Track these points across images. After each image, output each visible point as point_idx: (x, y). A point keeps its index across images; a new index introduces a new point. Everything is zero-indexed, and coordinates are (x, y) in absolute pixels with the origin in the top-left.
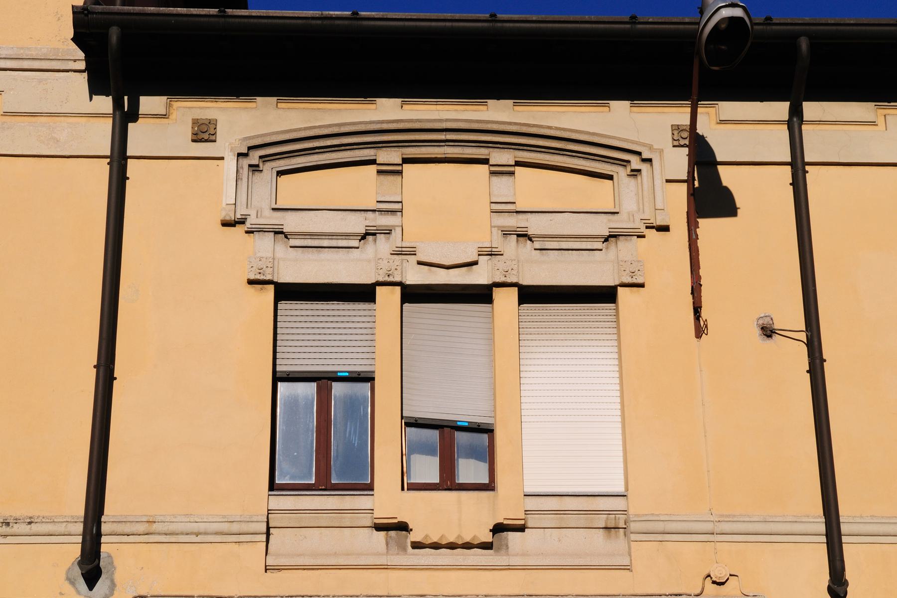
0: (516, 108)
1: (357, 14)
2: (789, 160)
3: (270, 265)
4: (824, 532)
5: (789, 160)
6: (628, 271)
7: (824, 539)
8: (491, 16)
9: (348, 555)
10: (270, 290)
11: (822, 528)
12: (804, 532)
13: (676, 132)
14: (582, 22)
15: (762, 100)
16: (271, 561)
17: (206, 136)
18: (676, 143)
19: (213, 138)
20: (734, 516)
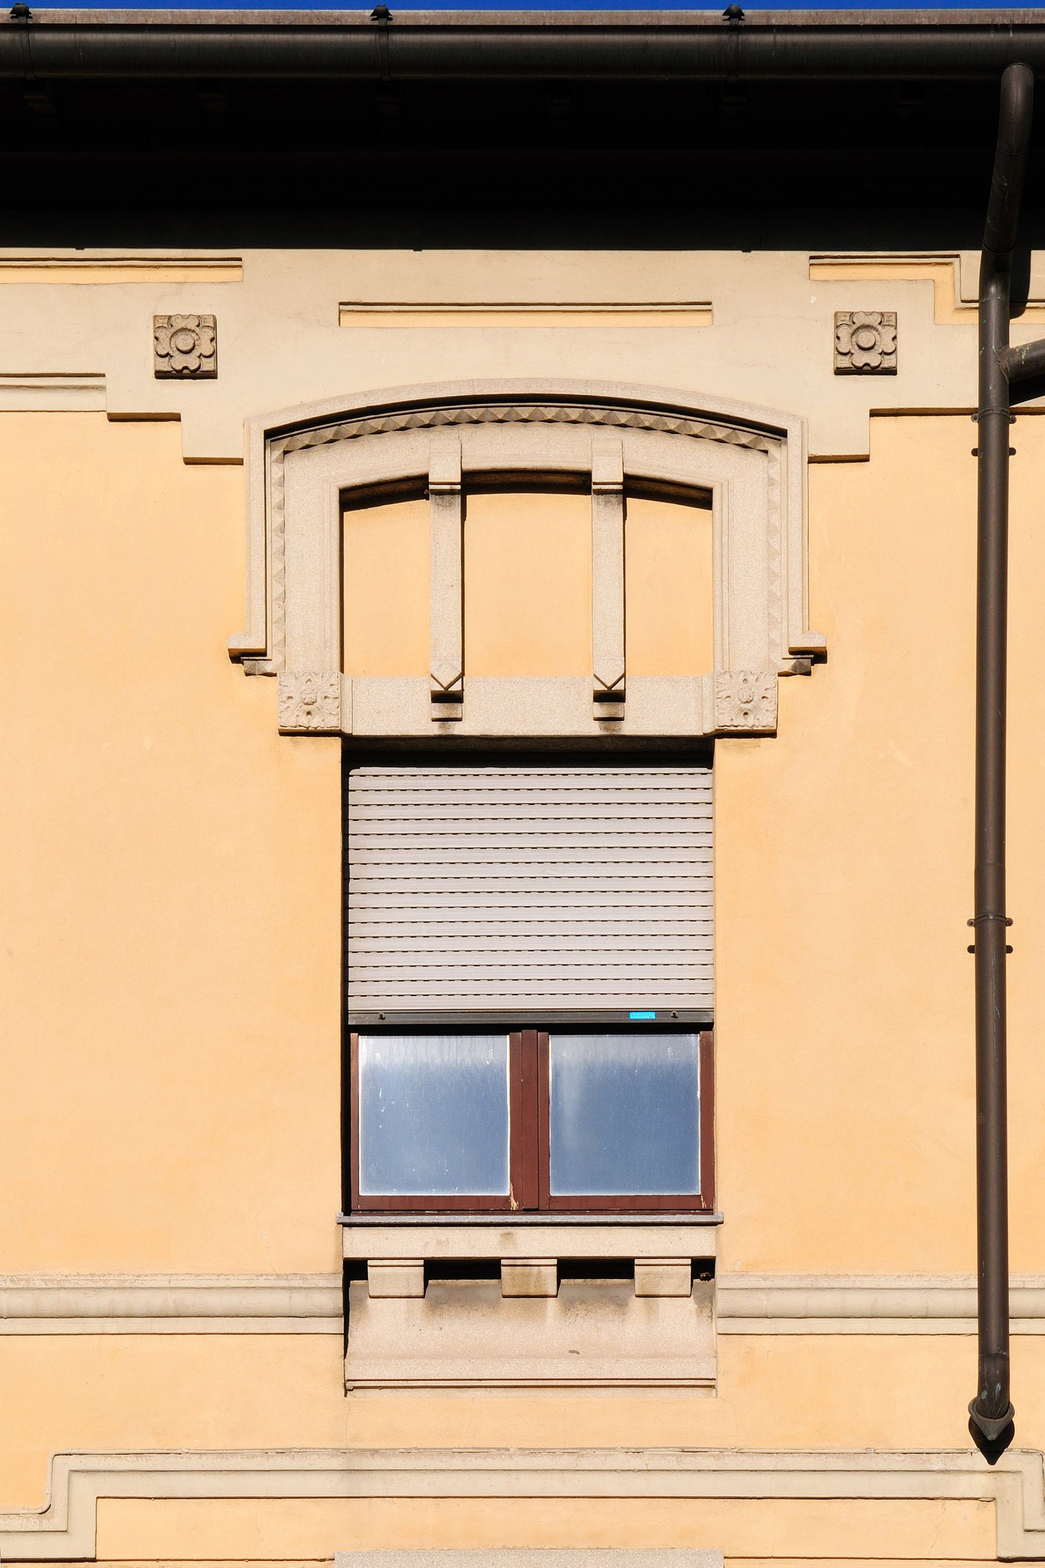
0: (820, 273)
1: (26, 14)
2: (975, 404)
3: (333, 692)
4: (976, 1313)
5: (975, 404)
6: (297, 699)
7: (974, 1326)
8: (17, 13)
9: (654, 1356)
10: (334, 748)
11: (971, 1302)
12: (63, 1310)
13: (845, 332)
14: (1004, 28)
15: (418, 244)
16: (357, 1371)
17: (192, 362)
18: (845, 363)
19: (207, 365)
20: (304, 1277)
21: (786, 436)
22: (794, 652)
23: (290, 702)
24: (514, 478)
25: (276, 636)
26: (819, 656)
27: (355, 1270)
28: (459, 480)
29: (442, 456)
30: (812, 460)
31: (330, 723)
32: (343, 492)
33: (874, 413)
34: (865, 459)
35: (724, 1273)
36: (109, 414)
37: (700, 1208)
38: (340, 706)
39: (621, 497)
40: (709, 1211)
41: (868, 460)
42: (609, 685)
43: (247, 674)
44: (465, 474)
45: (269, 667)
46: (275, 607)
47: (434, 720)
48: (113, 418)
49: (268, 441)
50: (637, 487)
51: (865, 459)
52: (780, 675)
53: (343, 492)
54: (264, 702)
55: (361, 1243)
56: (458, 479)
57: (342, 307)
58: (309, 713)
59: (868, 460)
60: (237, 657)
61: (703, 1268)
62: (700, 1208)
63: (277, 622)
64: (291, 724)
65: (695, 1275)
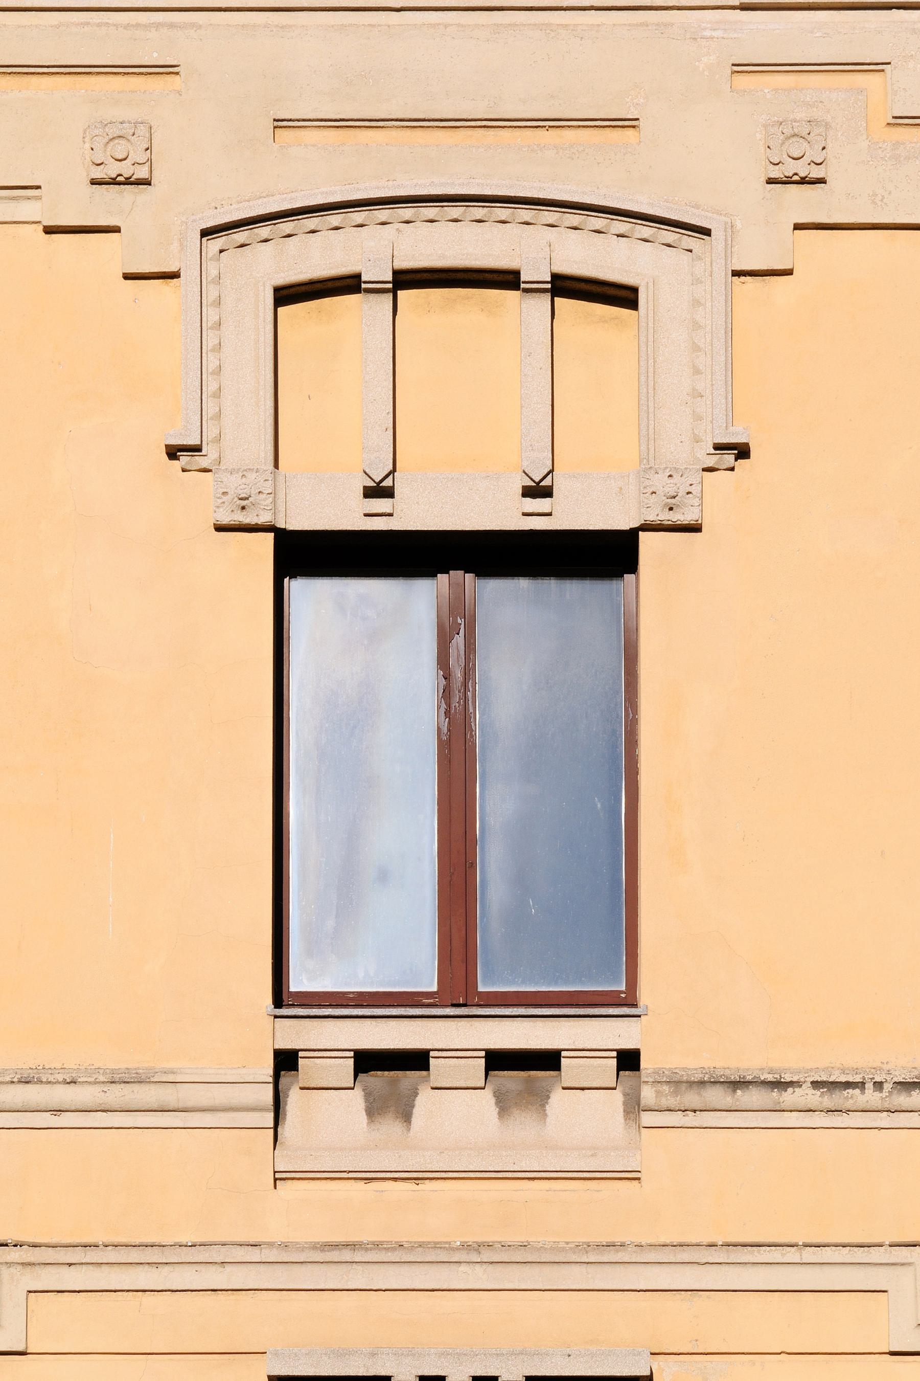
17: (126, 169)
21: (710, 235)
22: (718, 447)
23: (225, 498)
24: (443, 276)
25: (211, 432)
26: (743, 452)
27: (286, 1061)
28: (391, 279)
29: (375, 248)
30: (736, 274)
31: (264, 518)
32: (277, 290)
33: (797, 227)
34: (789, 272)
35: (646, 1080)
36: (45, 227)
37: (625, 1002)
38: (274, 502)
39: (548, 296)
40: (635, 1005)
41: (792, 274)
42: (537, 481)
43: (184, 470)
44: (396, 273)
45: (203, 462)
46: (211, 404)
47: (275, 1188)
48: (50, 230)
49: (204, 239)
50: (565, 286)
51: (789, 272)
52: (704, 470)
53: (277, 290)
54: (202, 497)
55: (292, 1034)
56: (389, 277)
57: (276, 124)
58: (243, 508)
59: (792, 274)
60: (173, 453)
61: (628, 1060)
62: (625, 1002)
63: (212, 419)
64: (226, 520)
65: (620, 1068)
